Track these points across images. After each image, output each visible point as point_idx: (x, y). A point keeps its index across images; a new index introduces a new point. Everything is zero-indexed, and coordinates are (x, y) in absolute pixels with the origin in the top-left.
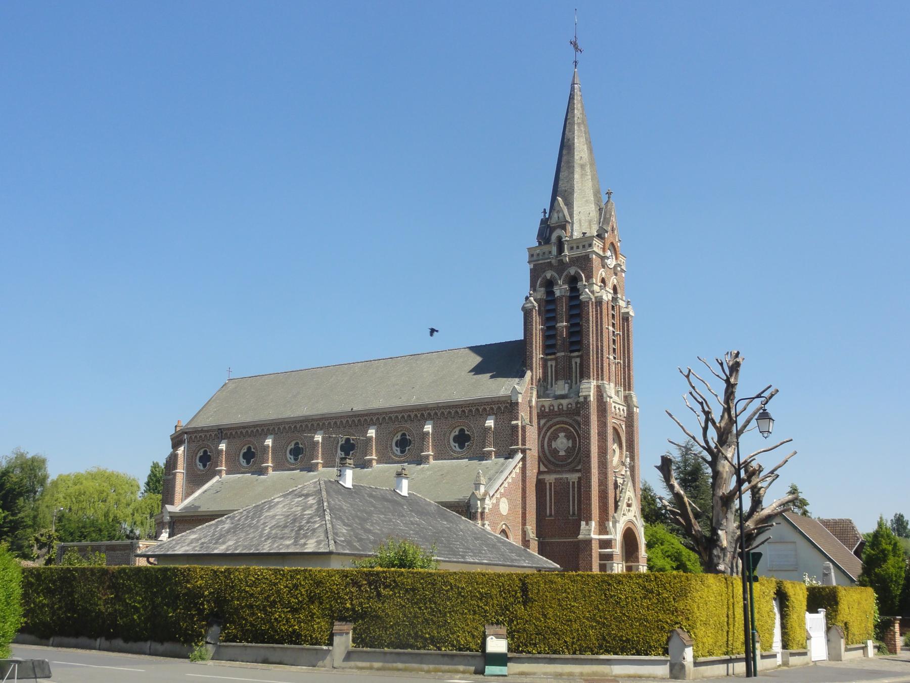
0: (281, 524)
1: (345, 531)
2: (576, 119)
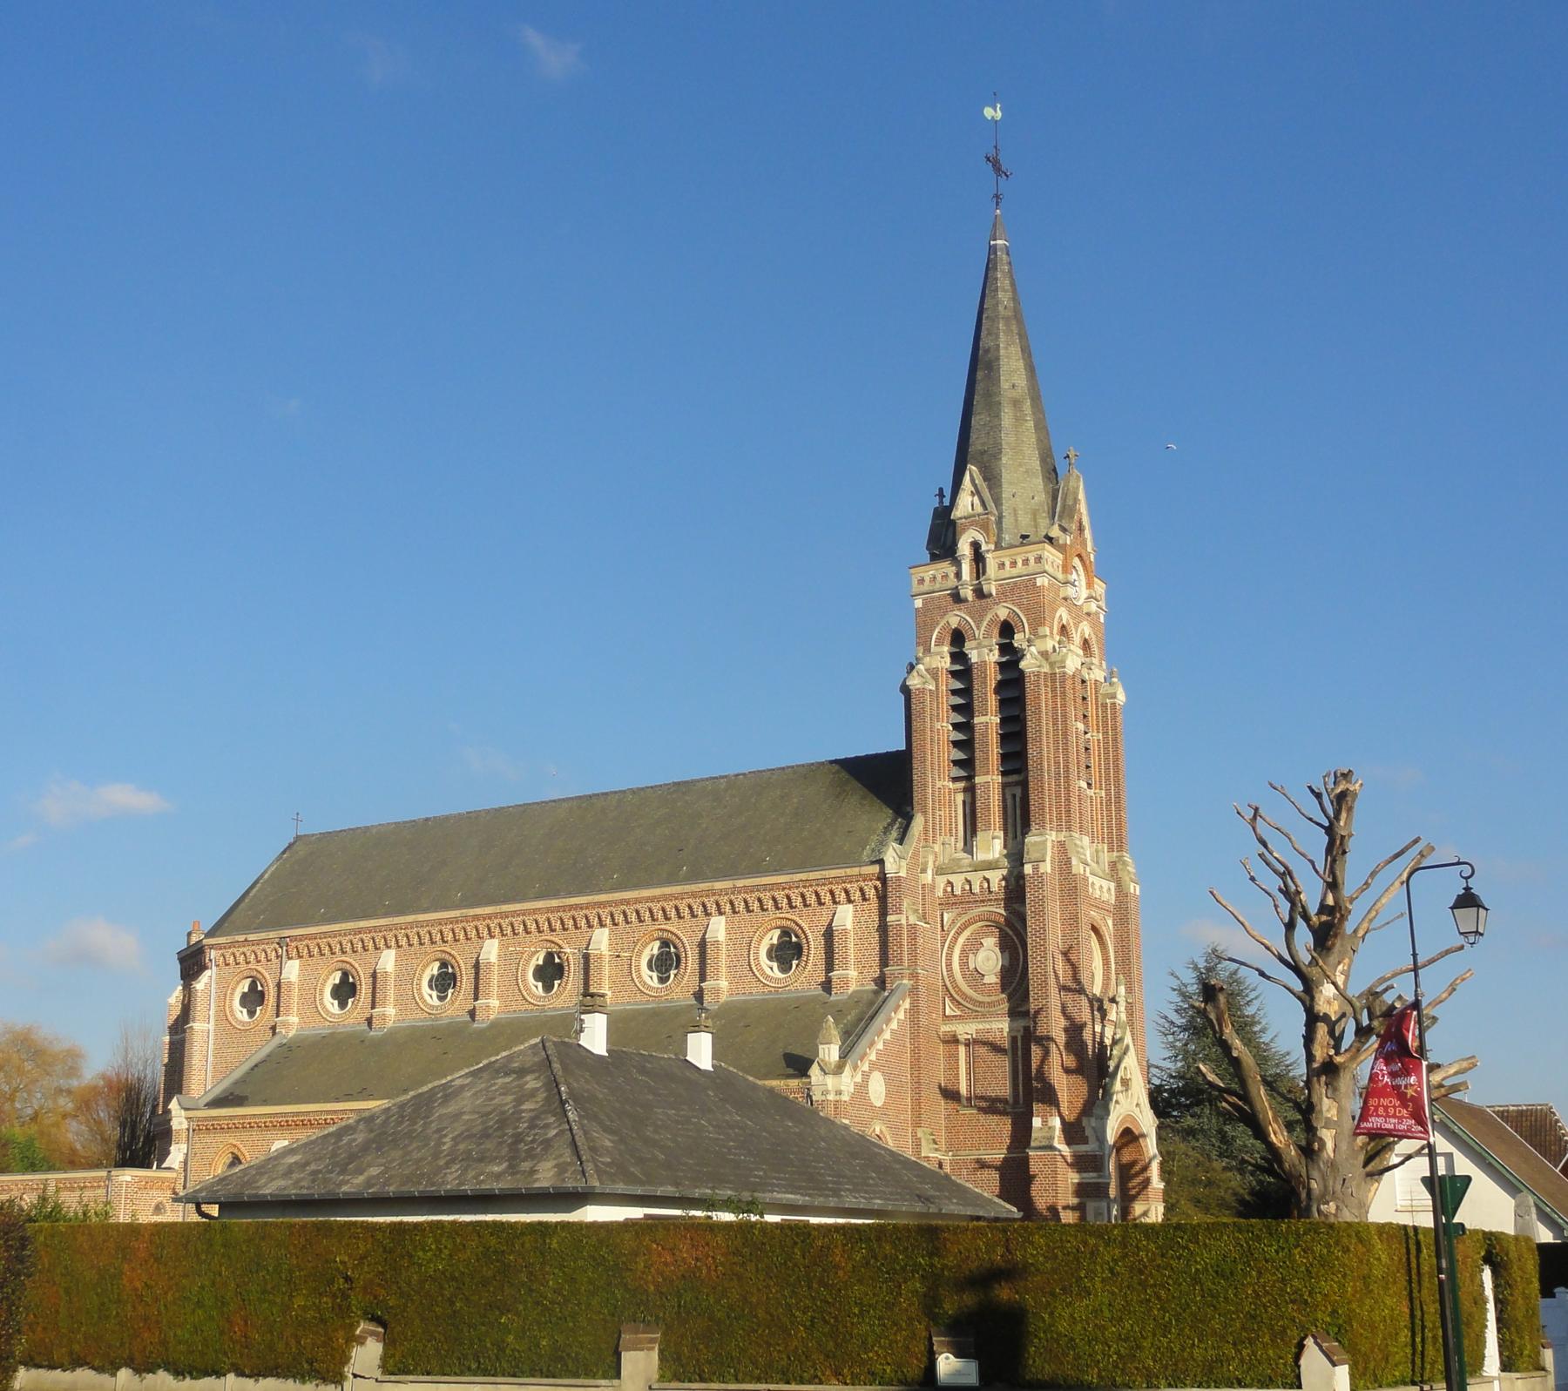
0: (474, 1131)
1: (608, 1144)
2: (1001, 308)
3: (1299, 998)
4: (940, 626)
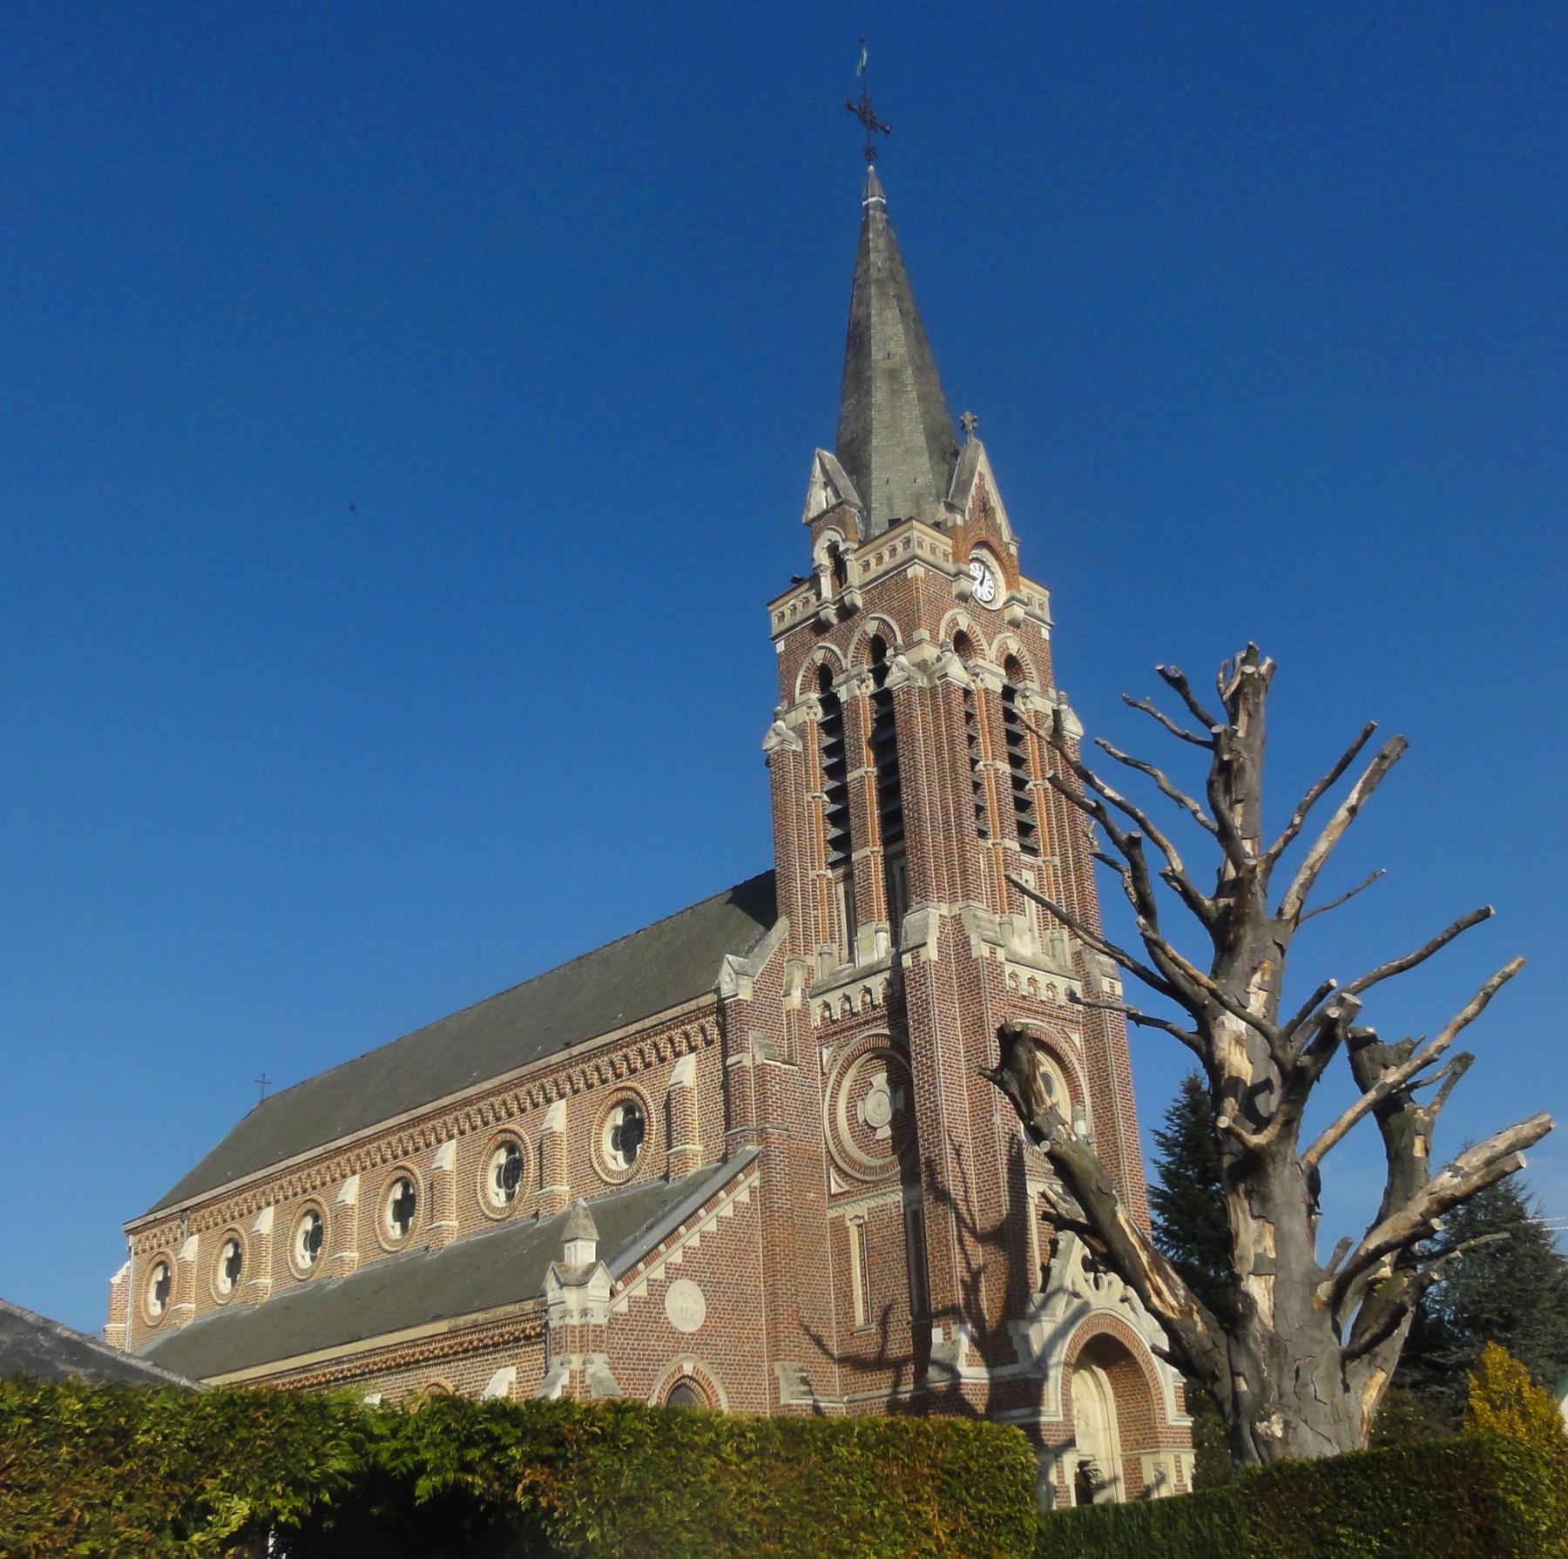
3: (1190, 1043)
4: (804, 668)
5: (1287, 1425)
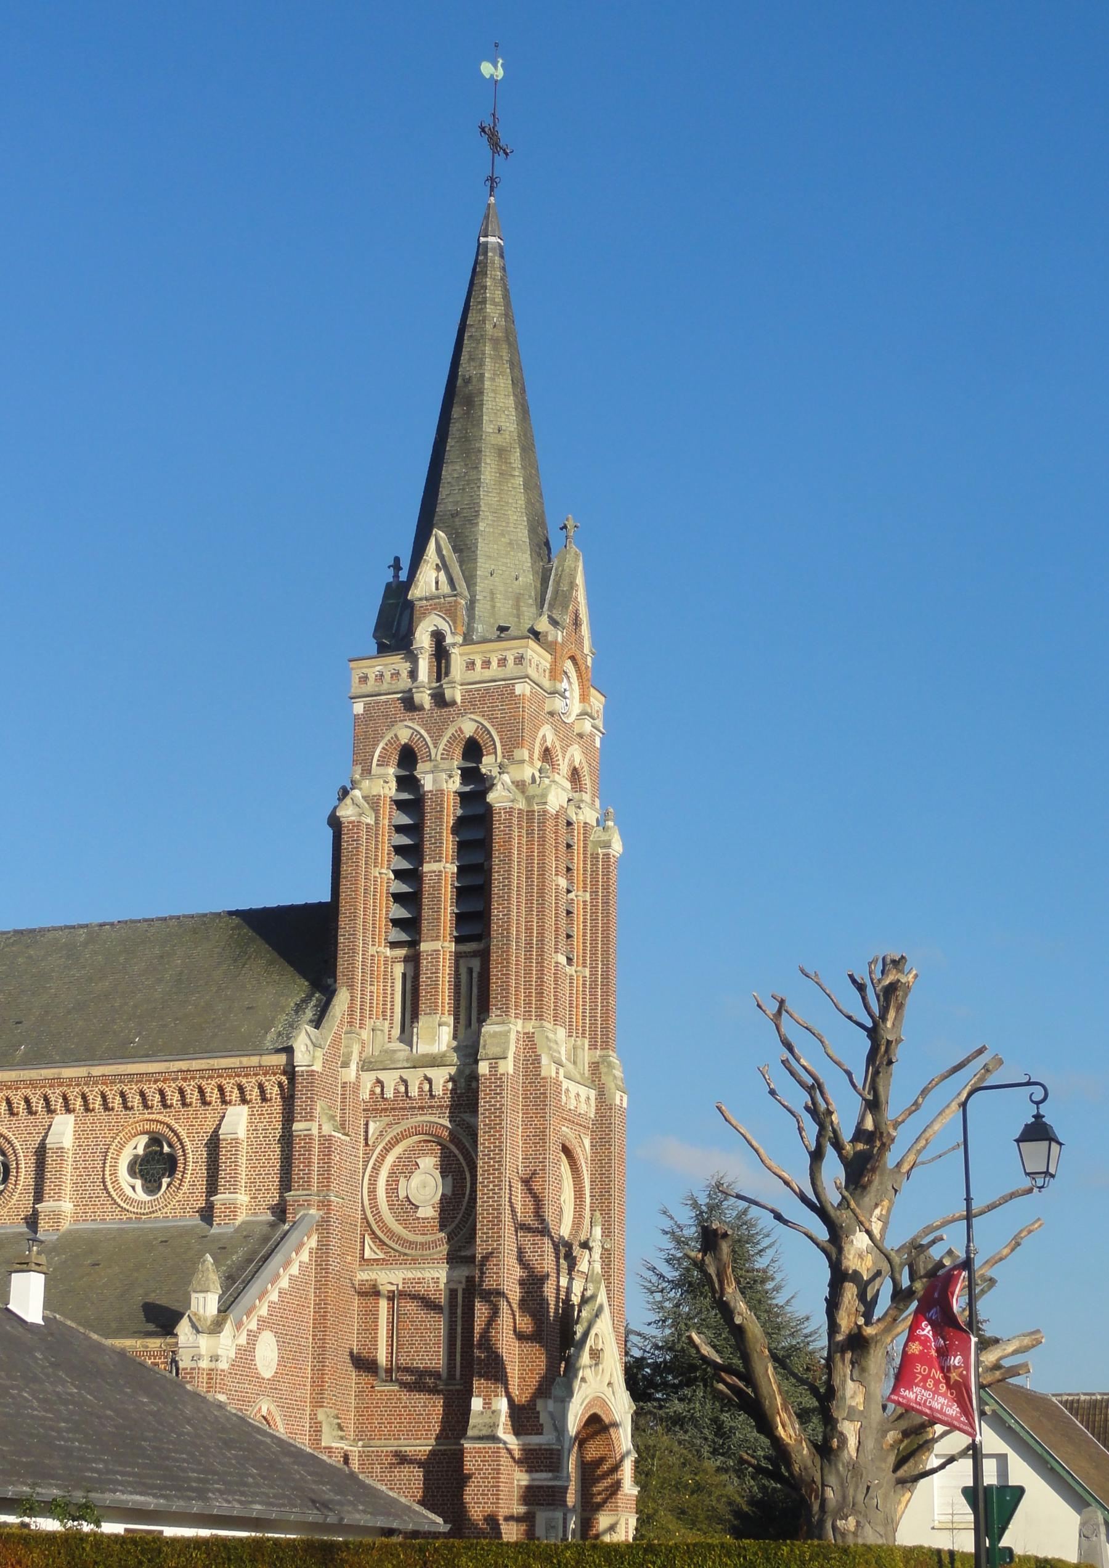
2: (489, 326)
3: (824, 1250)
4: (385, 741)
5: (858, 1523)
